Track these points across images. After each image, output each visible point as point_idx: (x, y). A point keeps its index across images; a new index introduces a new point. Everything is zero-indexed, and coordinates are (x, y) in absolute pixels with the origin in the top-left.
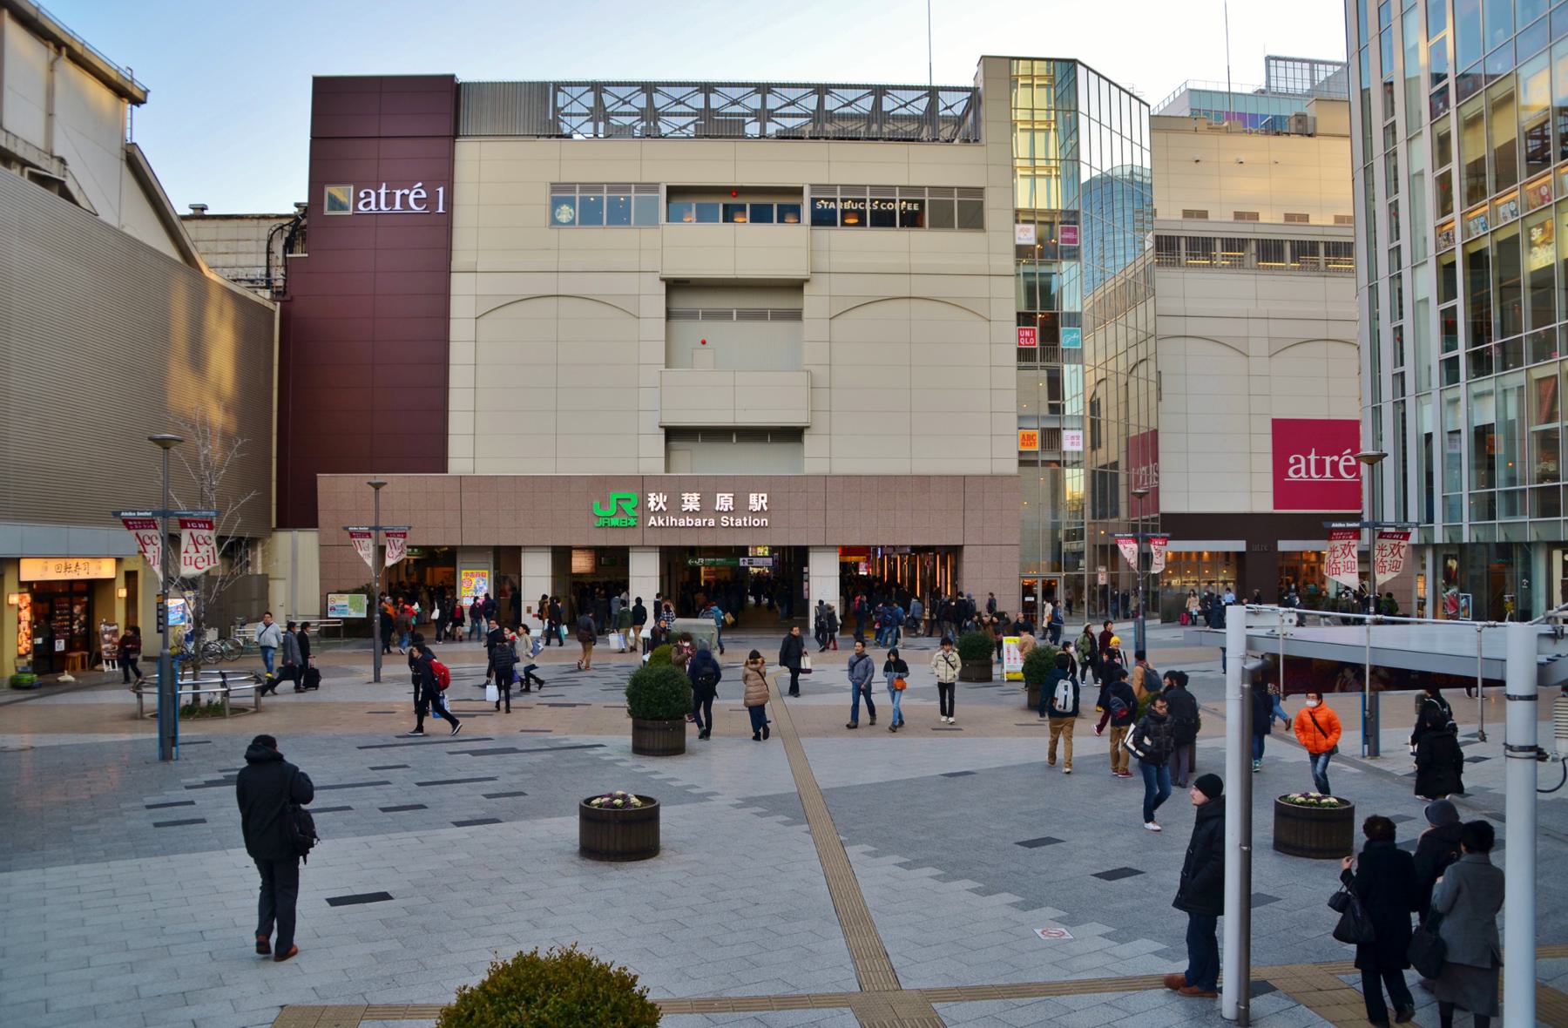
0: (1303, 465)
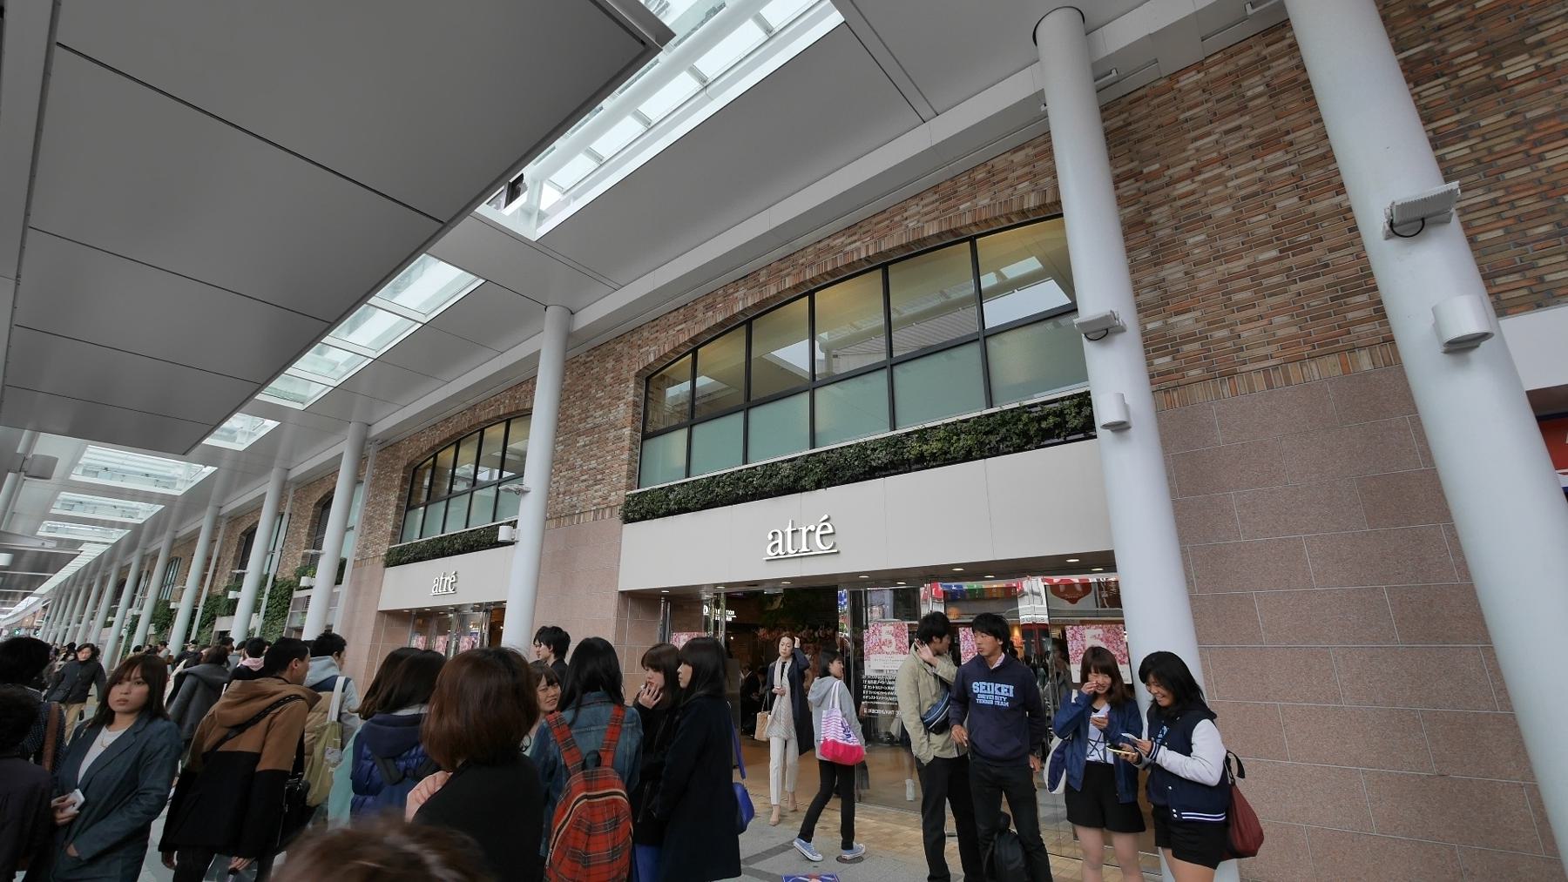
0: (780, 541)
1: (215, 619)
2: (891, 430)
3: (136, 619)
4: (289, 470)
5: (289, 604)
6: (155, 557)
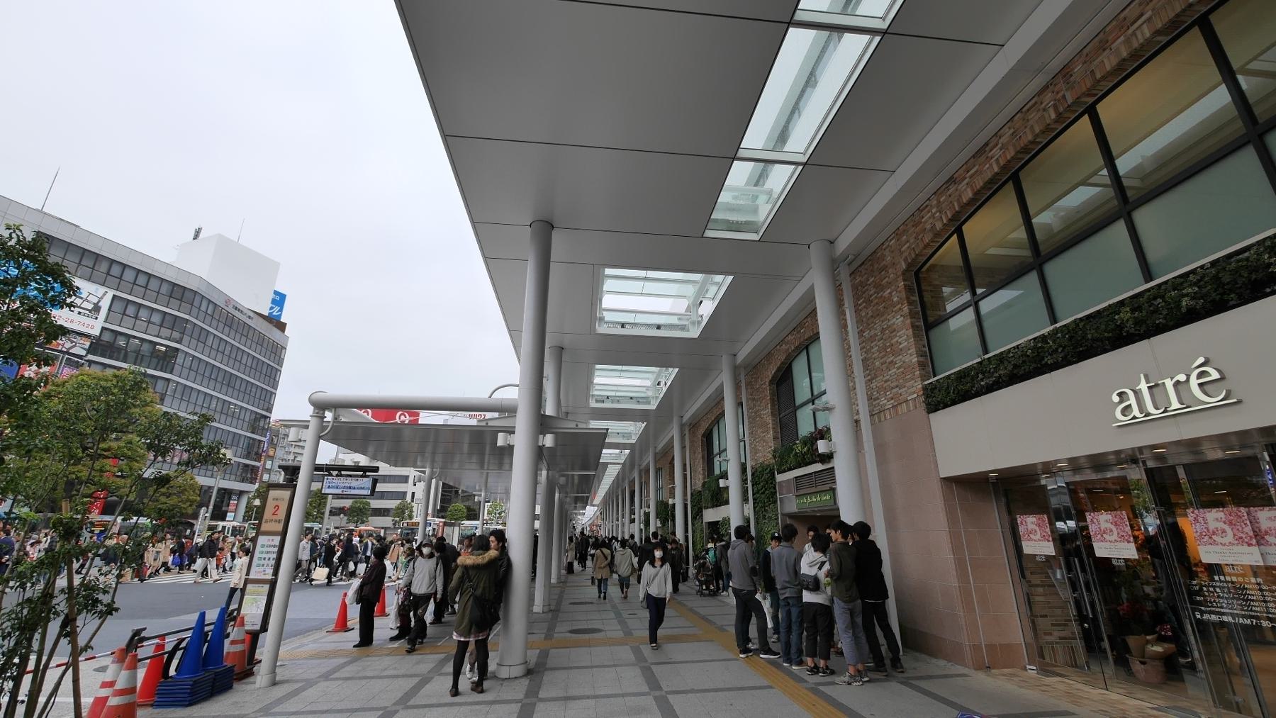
0: (1132, 400)
1: (702, 511)
2: (1147, 282)
3: (647, 515)
4: (735, 355)
5: (775, 488)
6: (648, 471)
